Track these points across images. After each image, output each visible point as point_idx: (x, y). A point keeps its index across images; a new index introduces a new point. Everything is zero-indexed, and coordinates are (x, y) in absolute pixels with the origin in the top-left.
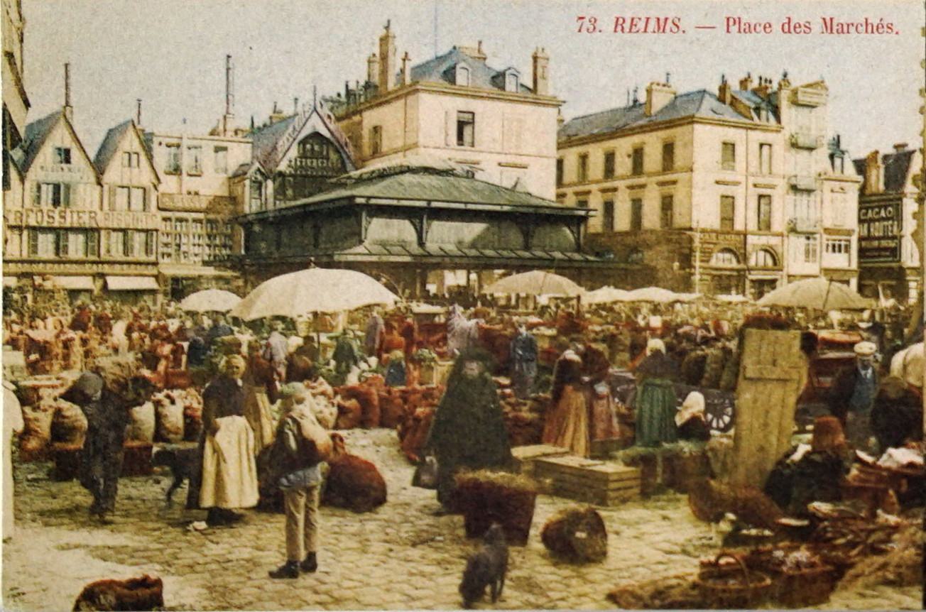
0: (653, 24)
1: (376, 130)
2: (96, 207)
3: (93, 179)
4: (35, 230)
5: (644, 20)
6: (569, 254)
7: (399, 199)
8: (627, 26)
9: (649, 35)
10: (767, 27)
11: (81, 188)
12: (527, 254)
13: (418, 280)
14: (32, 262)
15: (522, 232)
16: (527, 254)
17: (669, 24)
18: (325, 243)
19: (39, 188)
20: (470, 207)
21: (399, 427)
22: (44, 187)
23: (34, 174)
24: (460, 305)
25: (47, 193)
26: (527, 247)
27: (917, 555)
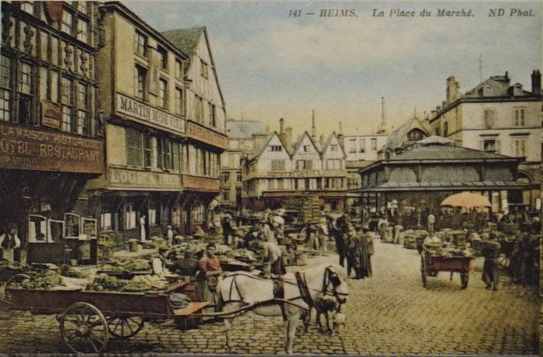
0: (340, 12)
1: (446, 124)
2: (320, 169)
3: (319, 158)
4: (296, 179)
5: (339, 15)
6: (508, 182)
7: (405, 160)
8: (327, 14)
9: (338, 17)
10: (413, 14)
11: (314, 161)
12: (480, 184)
13: (142, 195)
14: (326, 192)
15: (478, 172)
16: (480, 184)
17: (349, 13)
18: (29, 146)
19: (297, 163)
20: (445, 161)
21: (535, 260)
22: (299, 162)
23: (297, 157)
24: (91, 246)
25: (301, 164)
26: (481, 180)
27: (482, 125)
